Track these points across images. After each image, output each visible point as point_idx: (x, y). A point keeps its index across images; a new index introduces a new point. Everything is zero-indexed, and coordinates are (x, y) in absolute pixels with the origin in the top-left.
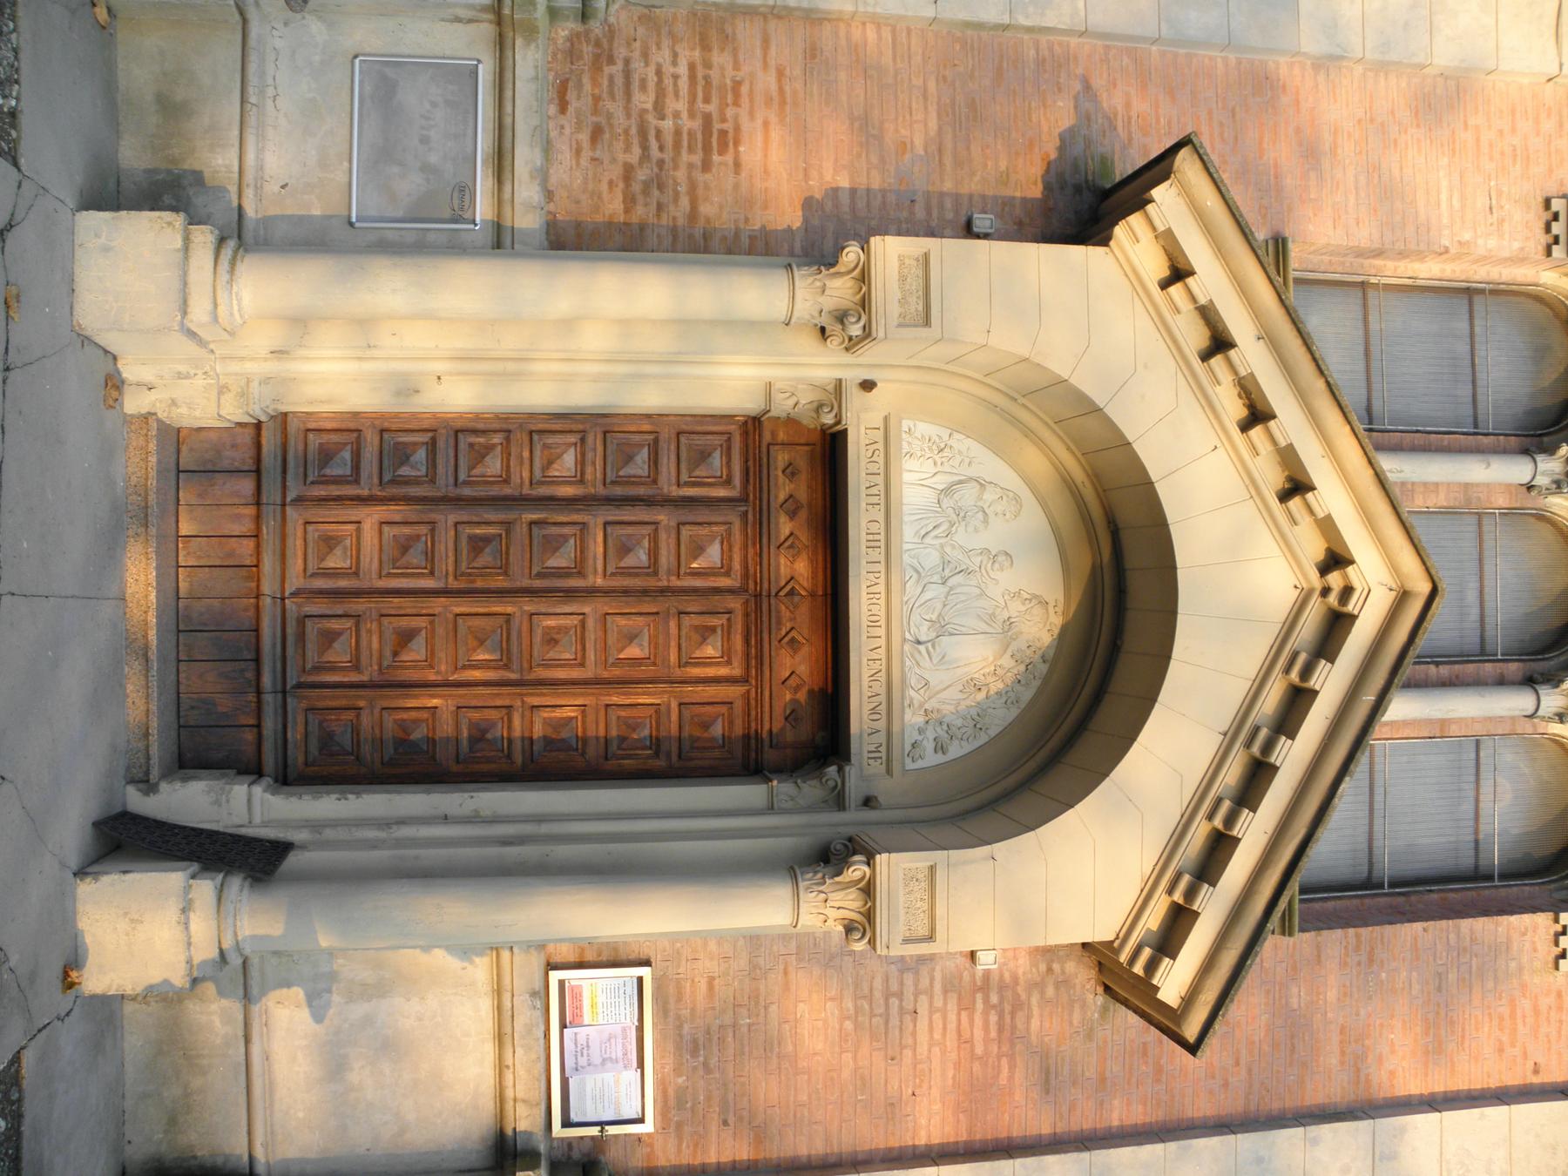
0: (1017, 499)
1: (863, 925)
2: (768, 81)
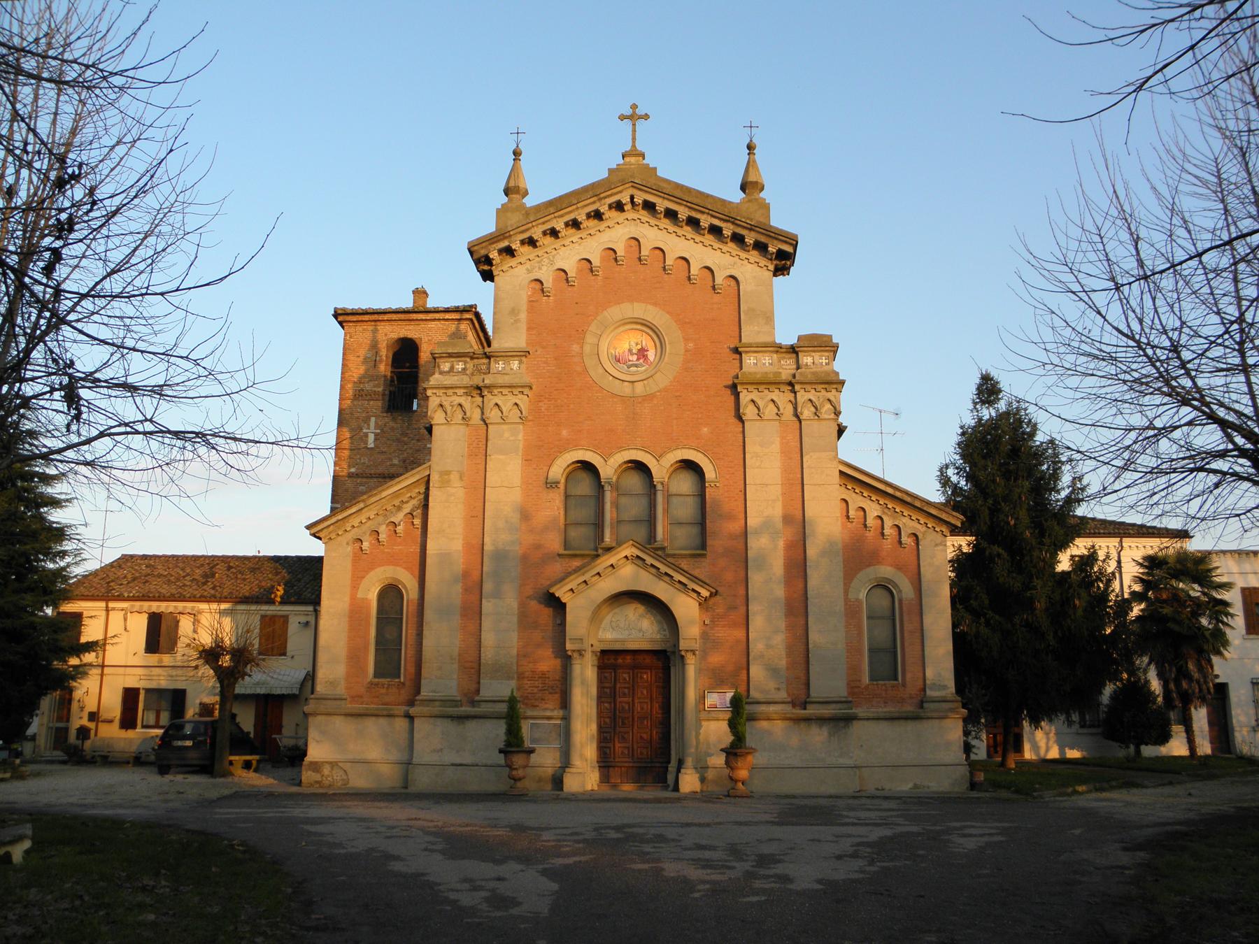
0: (615, 613)
1: (693, 652)
2: (531, 665)
